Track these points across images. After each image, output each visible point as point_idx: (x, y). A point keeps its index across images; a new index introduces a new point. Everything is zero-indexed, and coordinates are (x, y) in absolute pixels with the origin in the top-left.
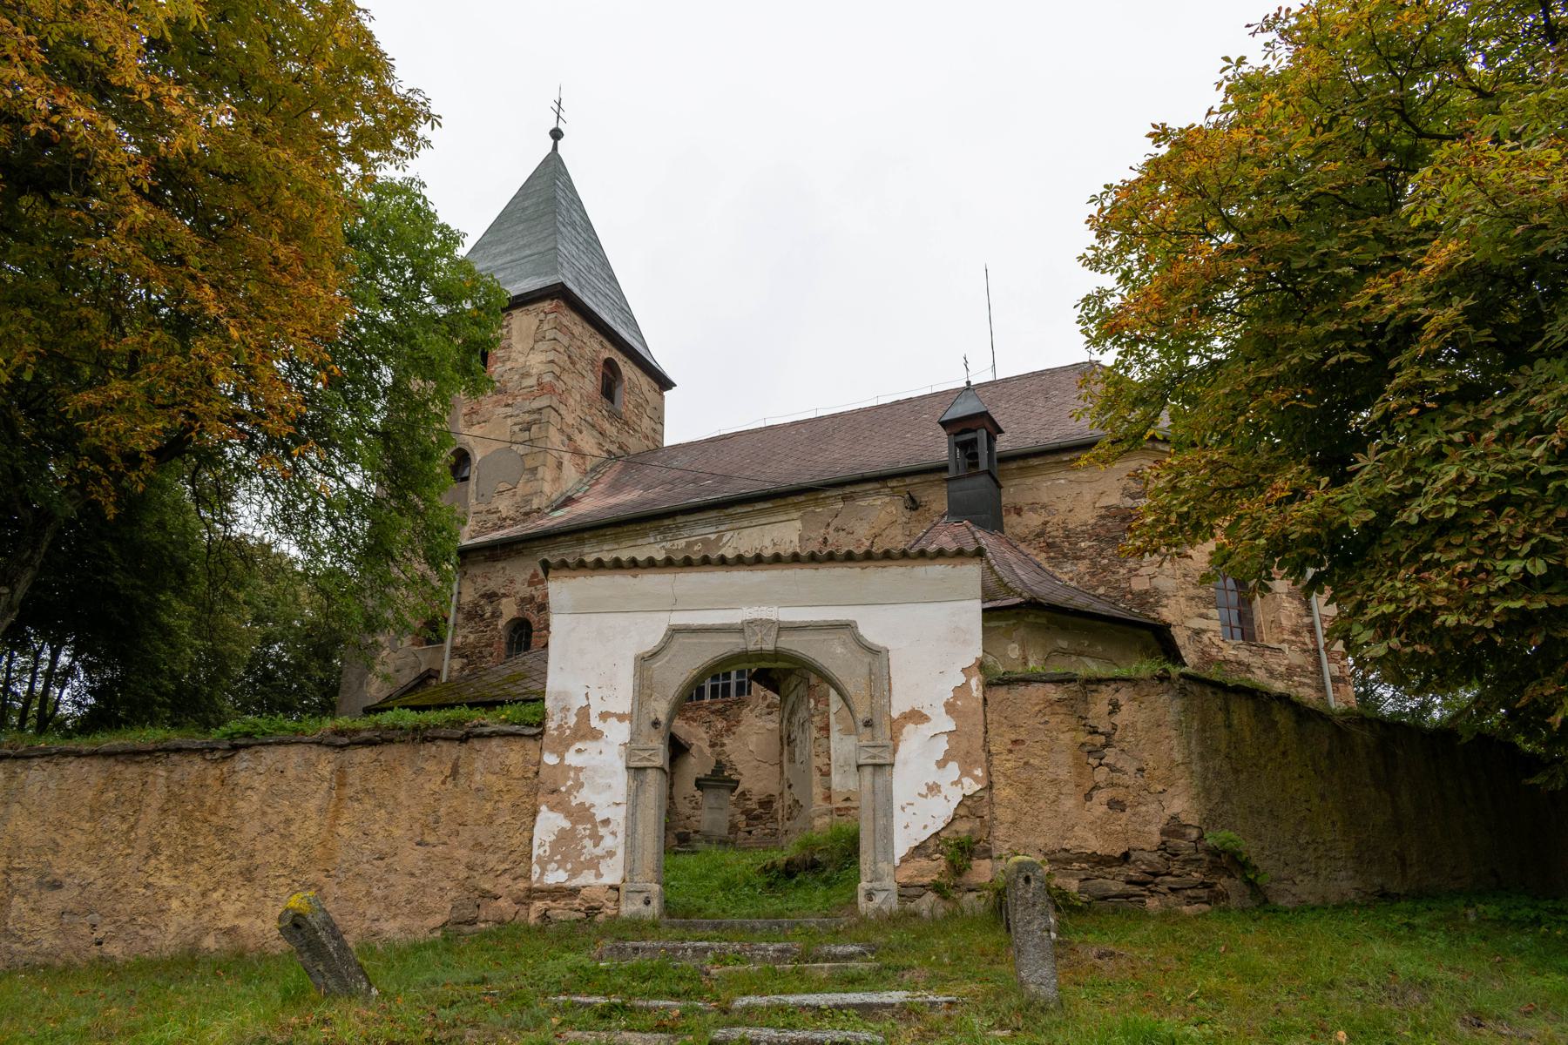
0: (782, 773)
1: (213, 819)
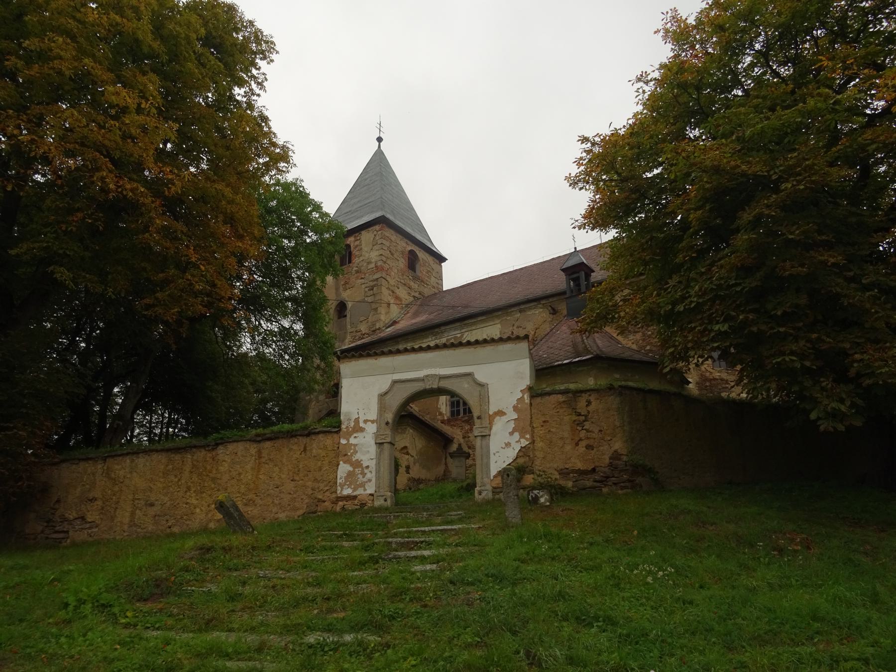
1: (210, 475)
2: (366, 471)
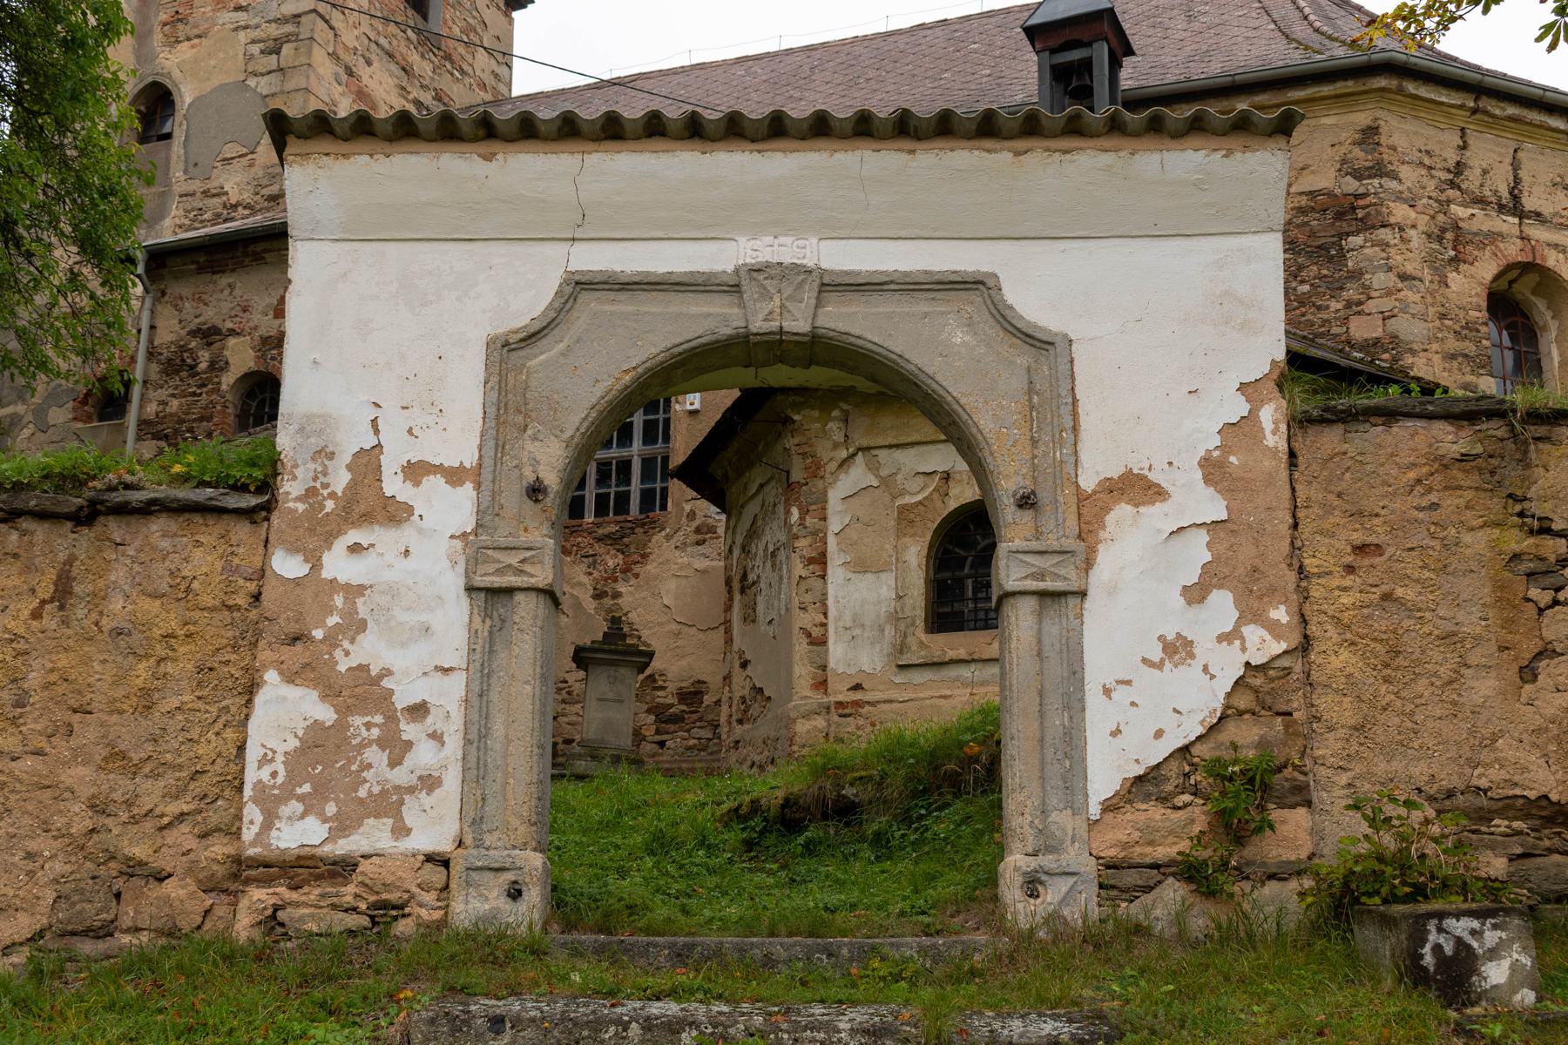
0: (729, 640)
2: (409, 730)
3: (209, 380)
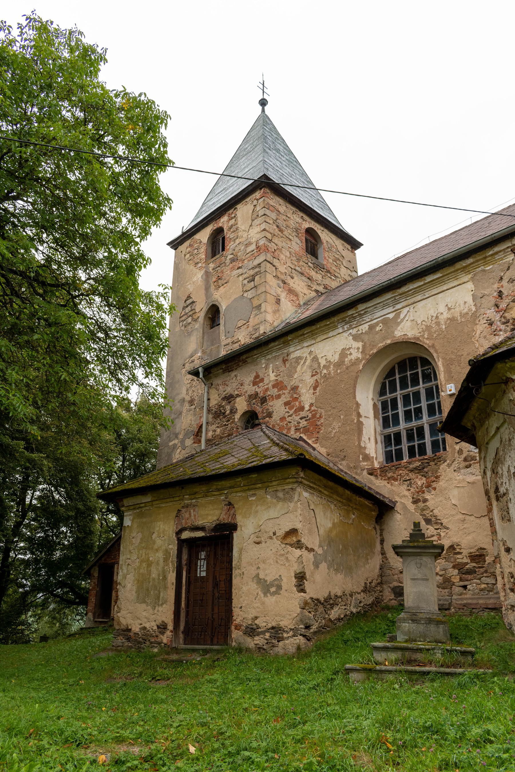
0: (494, 532)
3: (231, 418)
